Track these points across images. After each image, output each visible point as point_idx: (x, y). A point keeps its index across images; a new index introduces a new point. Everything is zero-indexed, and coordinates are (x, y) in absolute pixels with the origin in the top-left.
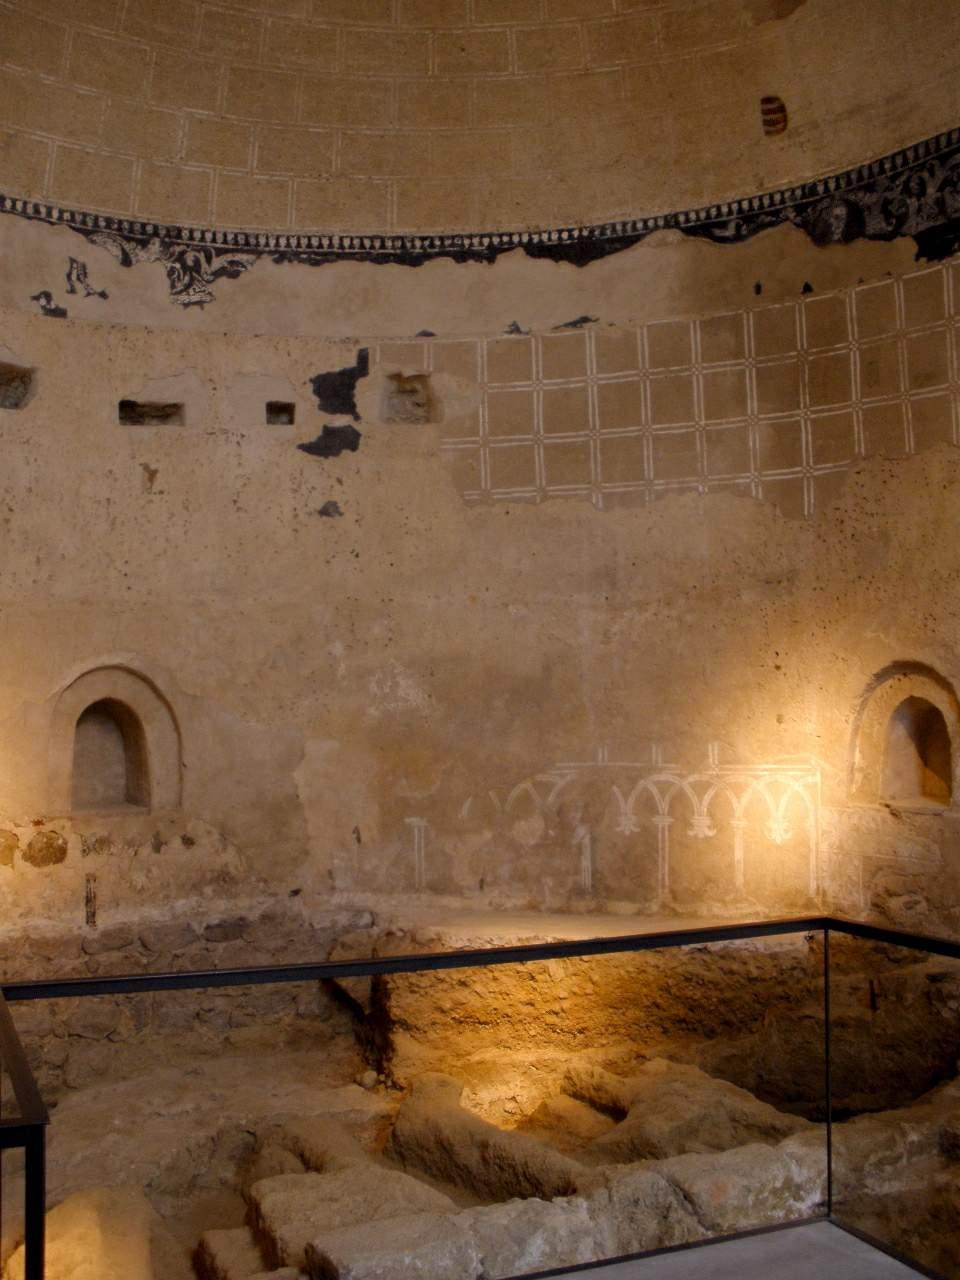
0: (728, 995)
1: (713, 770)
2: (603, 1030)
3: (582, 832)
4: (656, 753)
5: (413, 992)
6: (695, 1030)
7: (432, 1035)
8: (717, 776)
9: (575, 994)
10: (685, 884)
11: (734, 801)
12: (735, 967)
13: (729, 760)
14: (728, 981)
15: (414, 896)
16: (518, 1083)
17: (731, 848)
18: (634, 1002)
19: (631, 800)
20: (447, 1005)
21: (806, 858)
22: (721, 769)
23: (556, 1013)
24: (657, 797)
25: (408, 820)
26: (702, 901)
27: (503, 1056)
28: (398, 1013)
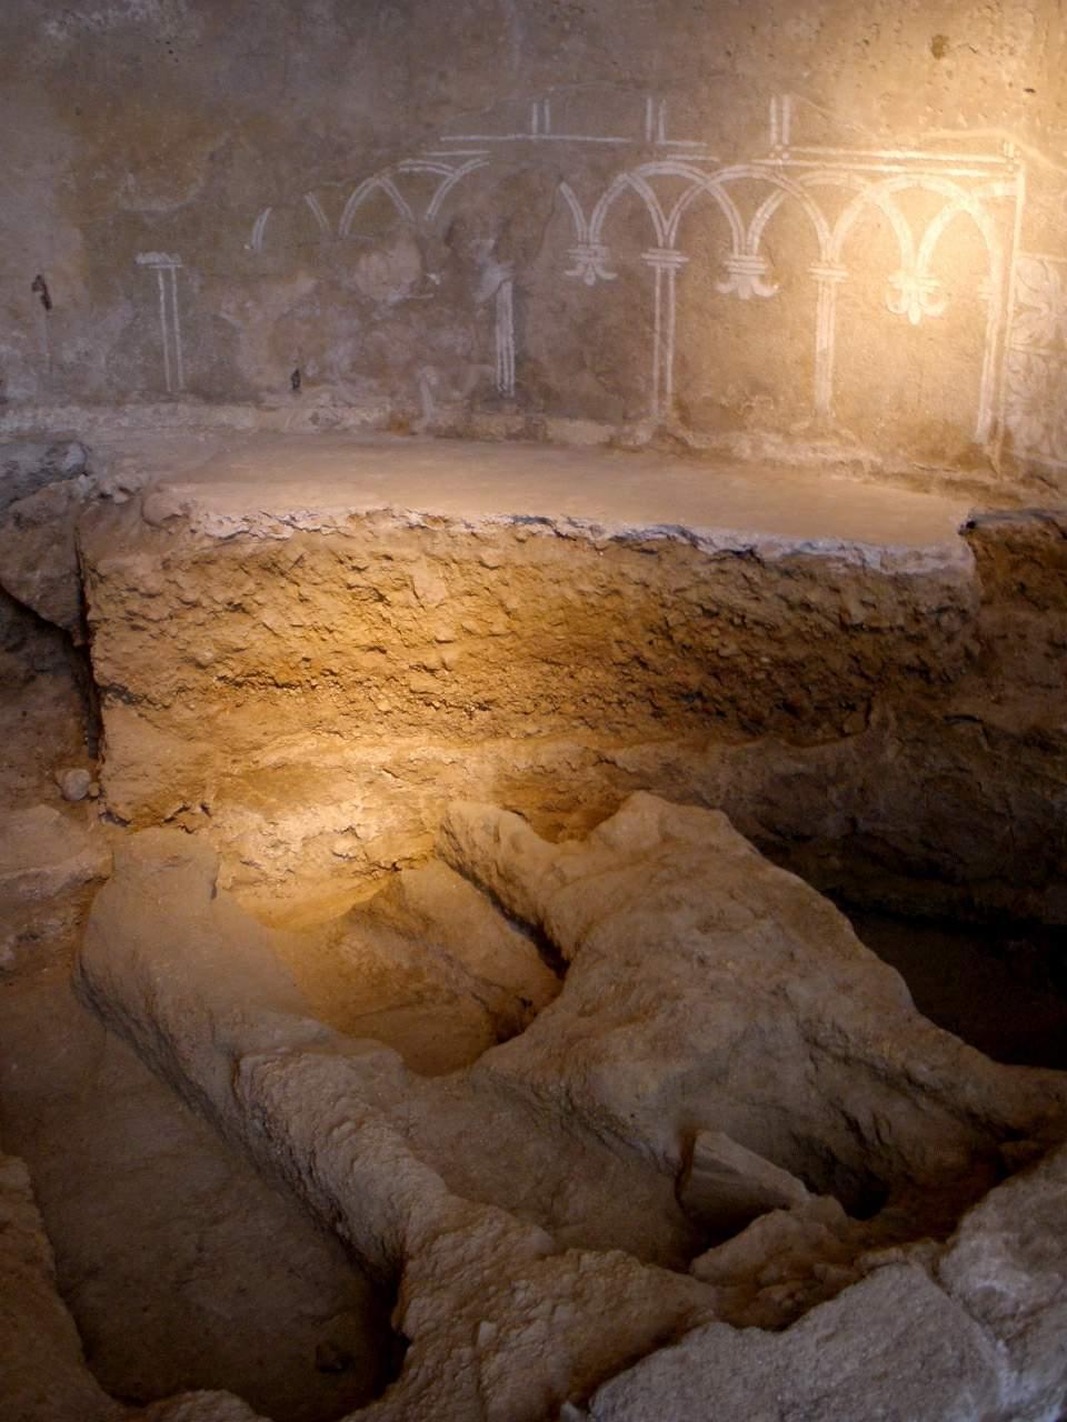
0: (797, 652)
1: (778, 156)
2: (530, 708)
3: (496, 277)
4: (655, 116)
5: (135, 628)
6: (721, 714)
7: (181, 713)
8: (787, 170)
9: (469, 632)
10: (708, 394)
11: (822, 226)
12: (814, 597)
13: (814, 135)
14: (795, 622)
15: (165, 408)
16: (357, 801)
17: (810, 325)
18: (594, 653)
19: (599, 214)
20: (207, 655)
21: (975, 358)
22: (796, 156)
23: (432, 671)
24: (654, 209)
25: (142, 259)
26: (743, 428)
27: (328, 751)
28: (107, 674)
